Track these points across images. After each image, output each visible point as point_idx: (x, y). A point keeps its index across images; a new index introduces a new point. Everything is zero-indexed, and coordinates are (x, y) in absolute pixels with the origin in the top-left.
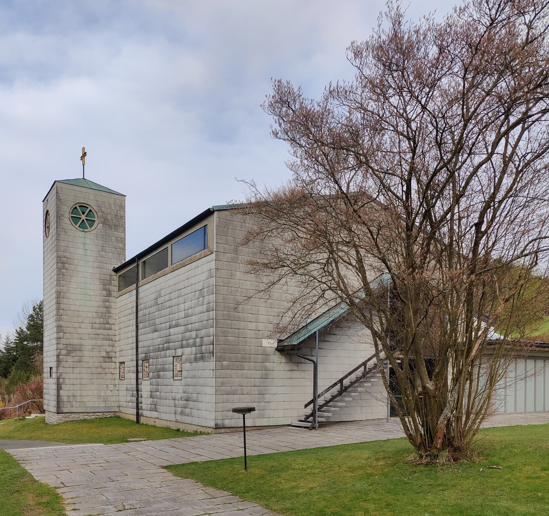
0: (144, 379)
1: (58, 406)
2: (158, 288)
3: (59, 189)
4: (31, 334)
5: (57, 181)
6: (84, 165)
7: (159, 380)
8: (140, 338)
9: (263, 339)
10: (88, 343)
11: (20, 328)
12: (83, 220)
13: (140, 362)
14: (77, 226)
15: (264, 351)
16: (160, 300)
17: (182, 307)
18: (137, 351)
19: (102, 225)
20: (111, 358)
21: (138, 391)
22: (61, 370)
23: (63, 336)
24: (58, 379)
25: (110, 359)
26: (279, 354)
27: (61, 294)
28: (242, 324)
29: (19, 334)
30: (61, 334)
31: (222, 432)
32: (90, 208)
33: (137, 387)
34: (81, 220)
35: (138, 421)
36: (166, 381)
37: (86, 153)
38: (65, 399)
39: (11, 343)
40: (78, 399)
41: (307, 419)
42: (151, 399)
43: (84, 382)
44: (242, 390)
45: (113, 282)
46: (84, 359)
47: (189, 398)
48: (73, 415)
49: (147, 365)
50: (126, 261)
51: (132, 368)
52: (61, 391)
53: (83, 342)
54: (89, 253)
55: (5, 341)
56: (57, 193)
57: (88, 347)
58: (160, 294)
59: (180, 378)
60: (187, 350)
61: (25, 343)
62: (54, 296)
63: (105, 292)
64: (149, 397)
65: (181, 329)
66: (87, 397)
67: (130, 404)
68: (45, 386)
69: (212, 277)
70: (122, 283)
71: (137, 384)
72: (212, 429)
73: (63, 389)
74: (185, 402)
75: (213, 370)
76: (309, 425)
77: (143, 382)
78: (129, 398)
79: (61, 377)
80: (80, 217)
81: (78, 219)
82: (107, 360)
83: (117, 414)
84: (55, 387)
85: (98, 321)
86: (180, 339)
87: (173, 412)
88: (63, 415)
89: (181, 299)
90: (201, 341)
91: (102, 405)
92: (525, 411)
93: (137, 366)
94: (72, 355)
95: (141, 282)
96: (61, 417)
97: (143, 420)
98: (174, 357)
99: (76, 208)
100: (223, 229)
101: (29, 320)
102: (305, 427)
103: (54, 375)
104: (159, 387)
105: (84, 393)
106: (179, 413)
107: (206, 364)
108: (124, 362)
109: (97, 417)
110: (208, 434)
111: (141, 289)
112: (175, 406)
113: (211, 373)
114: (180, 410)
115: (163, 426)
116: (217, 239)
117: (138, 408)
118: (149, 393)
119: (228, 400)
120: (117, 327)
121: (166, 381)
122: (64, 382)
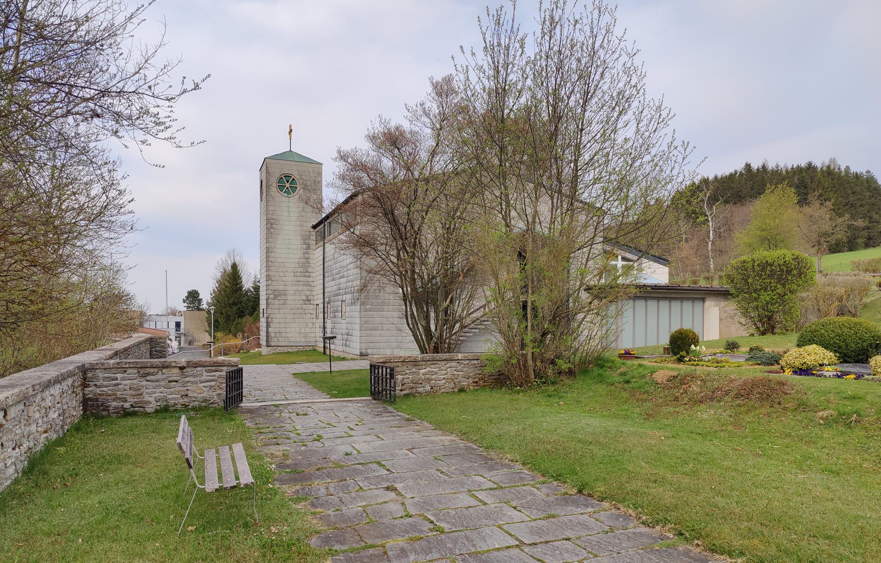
1: (267, 341)
3: (268, 164)
8: (326, 285)
10: (291, 289)
12: (287, 188)
13: (326, 304)
18: (324, 296)
22: (269, 311)
24: (267, 318)
32: (293, 177)
33: (324, 325)
38: (273, 335)
43: (288, 321)
46: (288, 302)
48: (279, 348)
53: (288, 288)
71: (324, 322)
82: (307, 302)
83: (315, 348)
85: (299, 270)
91: (303, 340)
92: (327, 338)
110: (355, 359)
113: (357, 314)
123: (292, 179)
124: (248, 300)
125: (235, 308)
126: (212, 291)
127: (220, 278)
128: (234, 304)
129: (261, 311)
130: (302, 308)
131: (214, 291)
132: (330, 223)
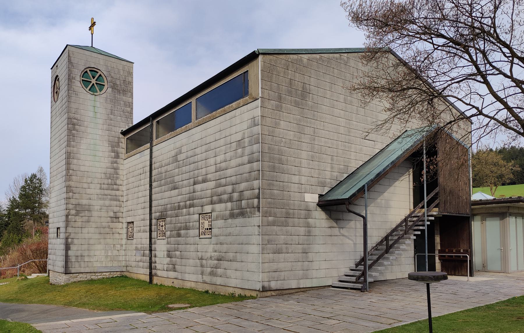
0: (158, 238)
2: (178, 145)
3: (71, 53)
4: (23, 203)
5: (69, 45)
6: (92, 34)
8: (154, 197)
9: (306, 194)
10: (97, 204)
11: (13, 197)
13: (154, 221)
14: (88, 89)
15: (307, 206)
16: (181, 157)
19: (111, 89)
20: (119, 218)
22: (70, 230)
23: (72, 196)
24: (67, 239)
25: (118, 219)
26: (320, 210)
27: (71, 155)
28: (285, 177)
29: (12, 202)
30: (71, 194)
31: (268, 295)
32: (100, 73)
33: (150, 247)
37: (95, 23)
38: (73, 259)
39: (4, 210)
40: (86, 259)
41: (359, 279)
42: (169, 259)
43: (92, 242)
44: (287, 248)
45: (120, 144)
47: (223, 257)
48: (81, 275)
50: (134, 124)
52: (69, 251)
53: (92, 202)
54: (98, 116)
56: (69, 56)
57: (96, 208)
59: (209, 236)
60: (219, 207)
61: (17, 210)
62: (64, 156)
63: (113, 154)
64: (166, 256)
65: (212, 184)
67: (141, 264)
68: (50, 246)
69: (255, 125)
70: (129, 146)
72: (258, 292)
73: (71, 249)
74: (216, 262)
75: (259, 226)
76: (359, 286)
77: (158, 242)
78: (139, 258)
79: (70, 237)
81: (88, 83)
82: (115, 220)
84: (63, 247)
85: (106, 181)
86: (209, 195)
87: (200, 272)
88: (71, 275)
89: (211, 153)
93: (151, 225)
94: (80, 215)
95: (155, 142)
96: (69, 277)
97: (155, 280)
98: (200, 214)
99: (86, 72)
100: (268, 72)
101: (21, 190)
102: (351, 289)
103: (62, 235)
105: (92, 253)
107: (247, 219)
108: (133, 222)
109: (104, 276)
111: (154, 149)
112: (202, 266)
114: (209, 270)
116: (262, 84)
117: (151, 268)
118: (166, 253)
119: (274, 260)
120: (124, 188)
121: (191, 240)
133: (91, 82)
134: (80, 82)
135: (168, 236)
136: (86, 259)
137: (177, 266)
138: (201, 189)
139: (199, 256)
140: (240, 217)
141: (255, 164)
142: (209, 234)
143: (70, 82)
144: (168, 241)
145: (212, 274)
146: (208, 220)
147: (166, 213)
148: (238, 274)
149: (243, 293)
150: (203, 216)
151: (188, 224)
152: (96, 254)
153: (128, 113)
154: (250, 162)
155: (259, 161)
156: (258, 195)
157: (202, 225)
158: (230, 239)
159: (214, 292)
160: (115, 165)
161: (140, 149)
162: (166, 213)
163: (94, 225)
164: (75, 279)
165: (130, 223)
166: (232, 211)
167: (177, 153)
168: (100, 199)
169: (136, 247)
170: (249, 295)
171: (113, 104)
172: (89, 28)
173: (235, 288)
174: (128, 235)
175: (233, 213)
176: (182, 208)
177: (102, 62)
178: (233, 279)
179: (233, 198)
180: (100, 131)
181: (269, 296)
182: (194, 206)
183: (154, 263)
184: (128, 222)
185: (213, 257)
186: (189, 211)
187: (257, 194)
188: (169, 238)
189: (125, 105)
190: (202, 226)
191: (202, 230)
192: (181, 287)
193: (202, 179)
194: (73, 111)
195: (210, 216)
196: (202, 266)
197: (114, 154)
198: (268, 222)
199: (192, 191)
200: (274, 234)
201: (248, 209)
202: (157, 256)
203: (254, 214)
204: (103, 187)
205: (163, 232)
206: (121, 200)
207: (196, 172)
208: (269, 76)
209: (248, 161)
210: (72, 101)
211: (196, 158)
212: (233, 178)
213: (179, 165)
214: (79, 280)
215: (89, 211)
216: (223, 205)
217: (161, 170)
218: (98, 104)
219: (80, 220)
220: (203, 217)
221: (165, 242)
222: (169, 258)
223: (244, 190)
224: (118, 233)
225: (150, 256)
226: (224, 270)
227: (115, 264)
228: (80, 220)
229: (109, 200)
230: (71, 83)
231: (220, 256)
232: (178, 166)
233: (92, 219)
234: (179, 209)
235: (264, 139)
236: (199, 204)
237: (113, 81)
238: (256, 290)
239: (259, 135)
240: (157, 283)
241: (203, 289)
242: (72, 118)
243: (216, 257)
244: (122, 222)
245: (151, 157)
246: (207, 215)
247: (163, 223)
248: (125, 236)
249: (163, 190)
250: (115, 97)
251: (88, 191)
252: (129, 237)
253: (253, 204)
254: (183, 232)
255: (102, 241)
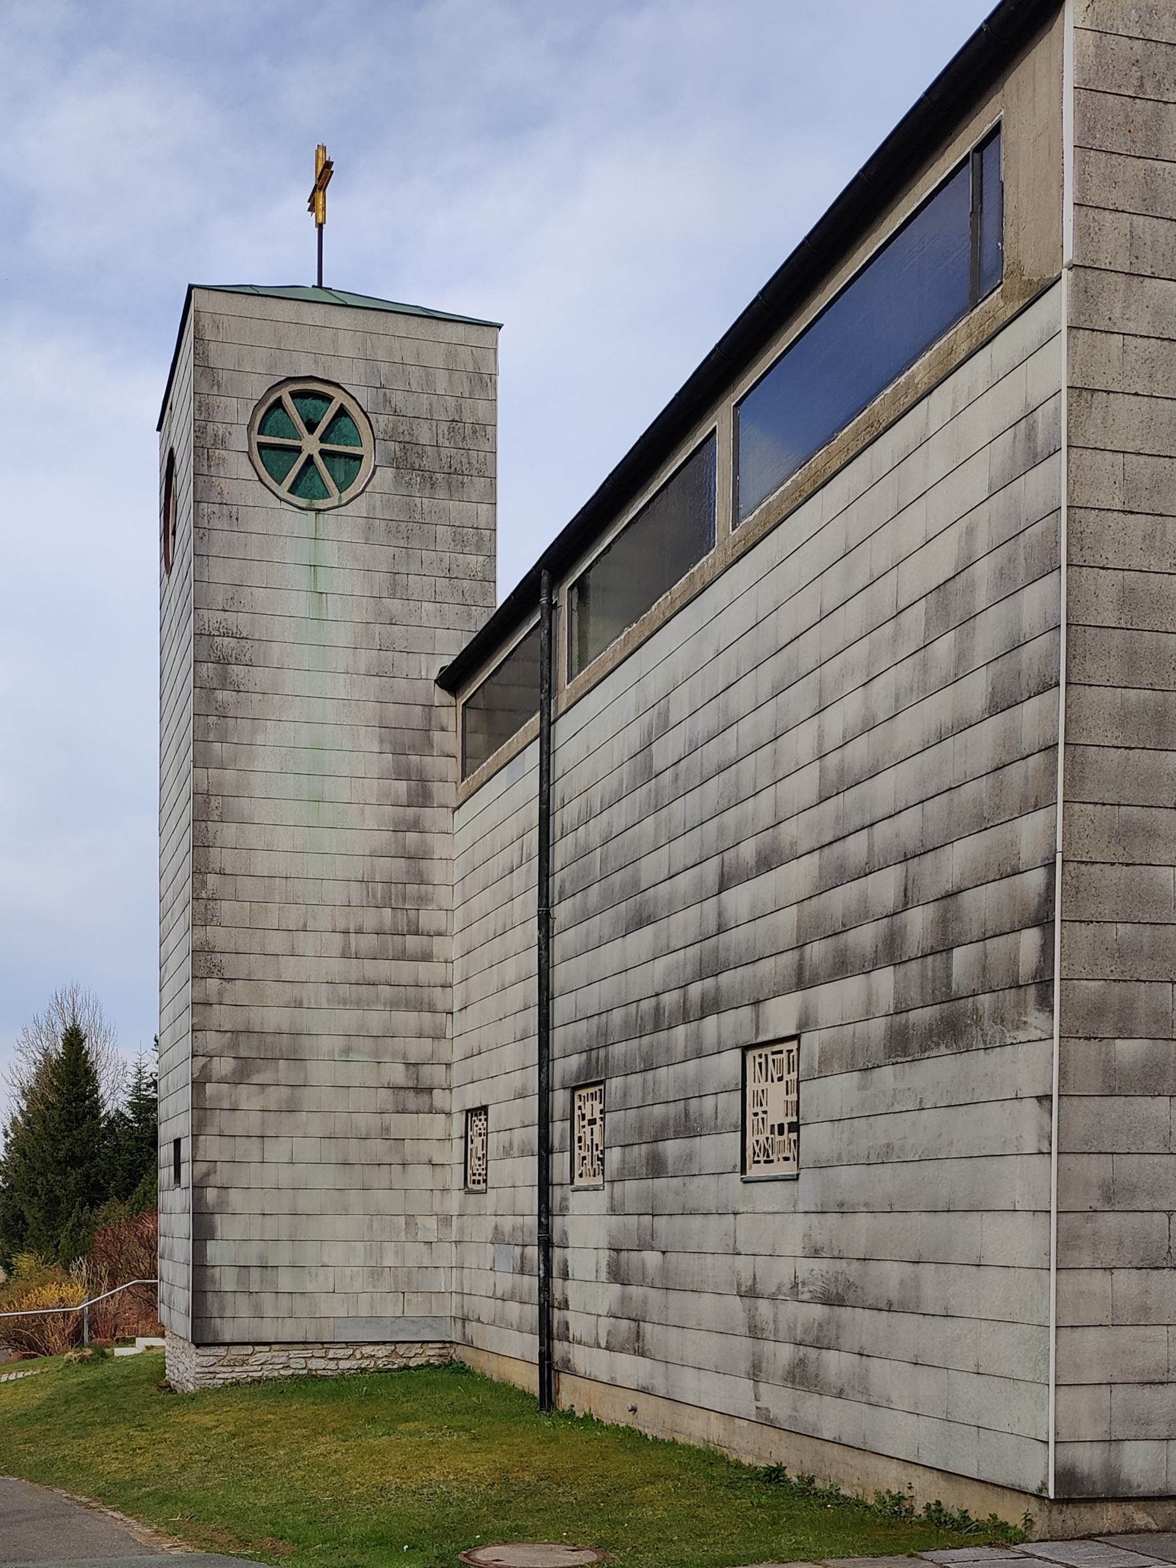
0: (578, 1182)
2: (654, 687)
3: (206, 321)
6: (320, 226)
7: (658, 1182)
8: (560, 975)
13: (560, 1099)
14: (283, 490)
16: (667, 749)
17: (801, 742)
21: (546, 1244)
22: (212, 1148)
23: (220, 993)
24: (198, 1188)
25: (426, 1097)
27: (213, 804)
30: (213, 984)
33: (544, 1228)
34: (302, 459)
35: (547, 1395)
36: (704, 1191)
38: (227, 1281)
40: (285, 1281)
42: (616, 1288)
43: (305, 1202)
45: (437, 736)
47: (850, 1285)
48: (263, 1354)
49: (592, 1108)
51: (518, 1135)
52: (211, 1247)
53: (313, 1021)
54: (333, 607)
55: (132, 1081)
57: (328, 1044)
58: (665, 716)
59: (789, 1169)
63: (402, 786)
64: (603, 1275)
66: (321, 1271)
67: (513, 1310)
69: (1035, 460)
71: (545, 1210)
72: (1034, 1506)
73: (218, 1235)
77: (576, 1201)
78: (506, 1281)
79: (212, 1180)
80: (296, 443)
81: (286, 457)
82: (412, 1100)
83: (460, 1353)
85: (370, 919)
86: (788, 938)
87: (744, 1366)
88: (222, 1351)
89: (800, 698)
90: (943, 923)
94: (255, 1079)
95: (566, 691)
96: (212, 1360)
97: (569, 1394)
98: (745, 1049)
99: (278, 404)
104: (661, 1222)
105: (310, 1254)
106: (780, 1372)
107: (980, 1062)
108: (484, 1109)
109: (364, 1364)
114: (783, 1354)
115: (681, 1439)
116: (1082, 180)
117: (546, 1332)
118: (604, 1256)
119: (1145, 1309)
120: (452, 947)
121: (704, 1191)
122: (222, 1202)
123: (333, 408)
124: (118, 1149)
125: (75, 1175)
126: (8, 1123)
127: (32, 1083)
128: (74, 1161)
129: (165, 1153)
130: (385, 1134)
131: (14, 1122)
132: (581, 586)
133: (298, 450)
134: (249, 454)
135: (615, 1172)
136: (285, 1281)
137: (647, 1328)
138: (753, 906)
139: (743, 1274)
140: (943, 1047)
141: (1031, 707)
142: (786, 1159)
143: (205, 463)
144: (612, 1198)
145: (797, 1380)
146: (786, 1077)
147: (607, 1056)
148: (927, 1383)
149: (955, 1500)
150: (763, 1060)
151: (694, 1103)
152: (326, 1261)
153: (473, 578)
154: (999, 705)
155: (1050, 687)
156: (1040, 906)
157: (759, 1109)
158: (886, 1180)
159: (811, 1480)
160: (411, 837)
161: (509, 746)
162: (607, 1056)
163: (316, 1125)
164: (237, 1369)
165: (476, 1115)
166: (897, 1018)
167: (650, 734)
168: (345, 1004)
169: (496, 1228)
170: (985, 1517)
171: (402, 543)
172: (309, 201)
173: (911, 1470)
174: (469, 1172)
175: (906, 1027)
176: (670, 1023)
177: (347, 347)
178: (900, 1415)
179: (903, 938)
180: (342, 682)
181: (1100, 1535)
182: (718, 1006)
183: (559, 1309)
184: (468, 1107)
185: (804, 1283)
186: (698, 1037)
187: (1036, 900)
188: (615, 1184)
189: (460, 542)
190: (756, 1114)
191: (756, 1137)
192: (667, 1437)
193: (759, 853)
194: (220, 602)
195: (795, 1053)
196: (755, 1332)
197: (409, 789)
198: (1105, 1072)
199: (712, 927)
200: (1152, 1145)
201: (985, 1000)
202: (570, 1276)
203: (1018, 1028)
204: (357, 944)
205: (595, 1153)
206: (440, 1007)
207: (730, 816)
208: (1139, 119)
209: (991, 702)
210: (214, 552)
211: (728, 746)
212: (909, 821)
213: (657, 792)
214: (255, 1374)
215: (296, 1059)
216: (851, 989)
217: (587, 834)
218: (329, 553)
219: (256, 1103)
220: (760, 1064)
221: (600, 1200)
222: (619, 1285)
223: (967, 884)
224: (426, 1160)
225: (542, 1275)
226: (858, 1357)
227: (416, 1307)
228: (256, 1103)
229: (385, 1006)
230: (209, 466)
231: (837, 1279)
232: (653, 803)
233: (309, 1098)
234: (657, 1029)
235: (1088, 541)
236: (742, 992)
237: (401, 430)
238: (1025, 1493)
239: (1058, 518)
240: (573, 1406)
241: (759, 1458)
242: (217, 633)
243: (817, 1287)
244: (447, 1109)
245: (545, 774)
246: (781, 1052)
247: (596, 1103)
248: (458, 1181)
249: (594, 938)
250: (411, 509)
251: (290, 968)
252: (474, 1182)
253: (1014, 961)
254: (672, 1148)
255: (354, 1197)
